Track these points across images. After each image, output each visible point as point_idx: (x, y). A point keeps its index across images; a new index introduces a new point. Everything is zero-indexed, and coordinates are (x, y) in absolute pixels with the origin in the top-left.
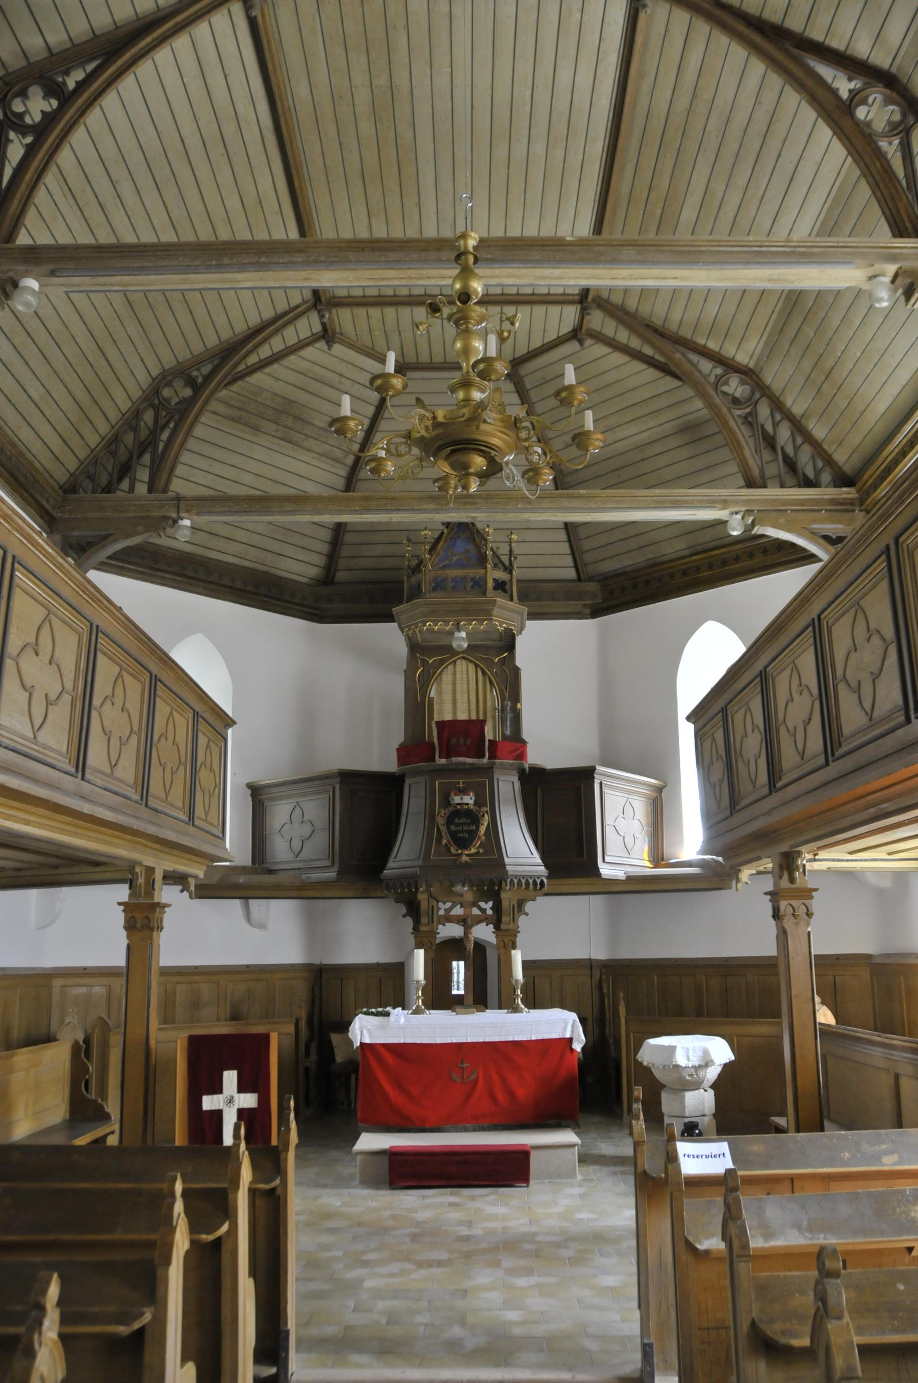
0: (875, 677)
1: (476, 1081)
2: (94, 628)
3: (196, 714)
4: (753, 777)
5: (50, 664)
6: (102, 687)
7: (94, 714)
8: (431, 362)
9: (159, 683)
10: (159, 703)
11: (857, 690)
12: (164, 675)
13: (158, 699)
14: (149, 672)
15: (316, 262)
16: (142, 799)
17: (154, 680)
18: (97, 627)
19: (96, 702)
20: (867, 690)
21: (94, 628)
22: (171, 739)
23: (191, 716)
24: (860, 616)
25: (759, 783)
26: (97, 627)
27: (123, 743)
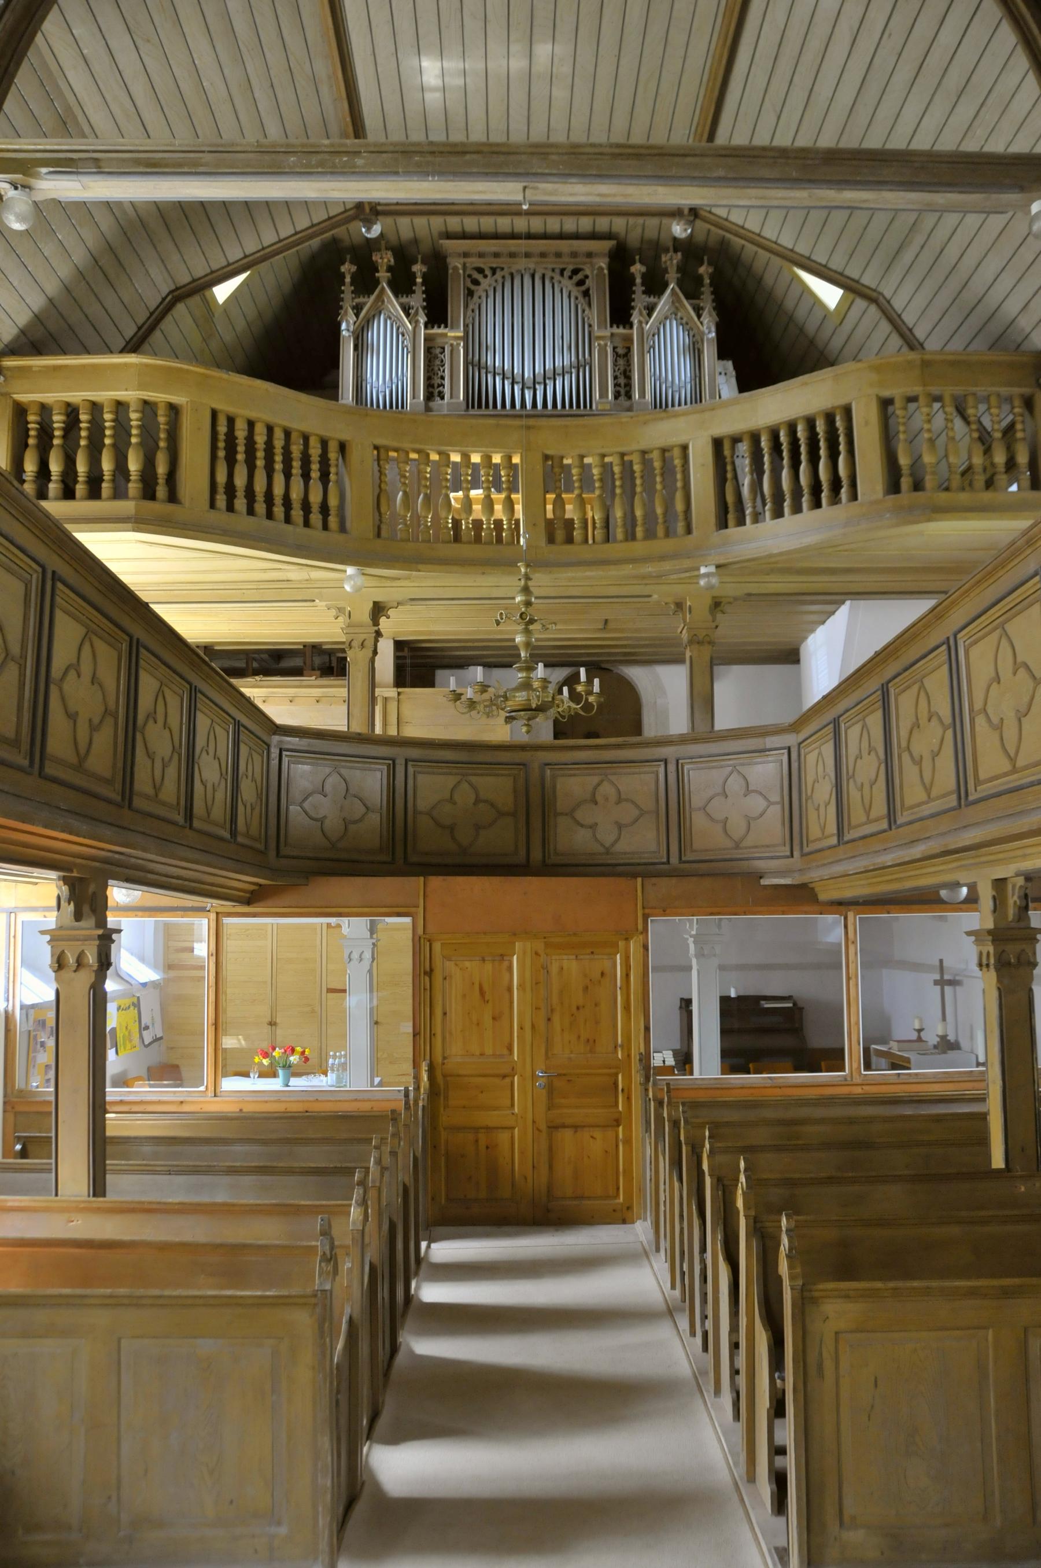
0: (935, 755)
1: (699, 316)
2: (49, 575)
3: (238, 724)
4: (867, 807)
5: (93, 683)
6: (62, 655)
7: (54, 691)
8: (557, 814)
9: (59, 585)
10: (199, 716)
11: (918, 762)
12: (139, 632)
13: (198, 713)
14: (128, 634)
15: (396, 173)
16: (123, 799)
17: (135, 647)
18: (138, 640)
19: (56, 671)
20: (927, 764)
21: (49, 575)
22: (250, 778)
23: (125, 646)
24: (1004, 642)
25: (874, 814)
26: (54, 572)
27: (93, 728)
